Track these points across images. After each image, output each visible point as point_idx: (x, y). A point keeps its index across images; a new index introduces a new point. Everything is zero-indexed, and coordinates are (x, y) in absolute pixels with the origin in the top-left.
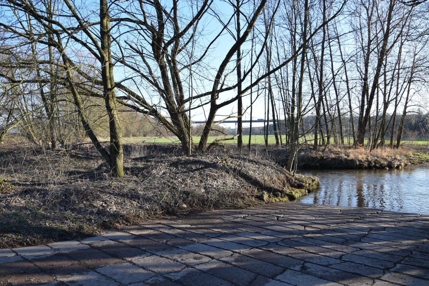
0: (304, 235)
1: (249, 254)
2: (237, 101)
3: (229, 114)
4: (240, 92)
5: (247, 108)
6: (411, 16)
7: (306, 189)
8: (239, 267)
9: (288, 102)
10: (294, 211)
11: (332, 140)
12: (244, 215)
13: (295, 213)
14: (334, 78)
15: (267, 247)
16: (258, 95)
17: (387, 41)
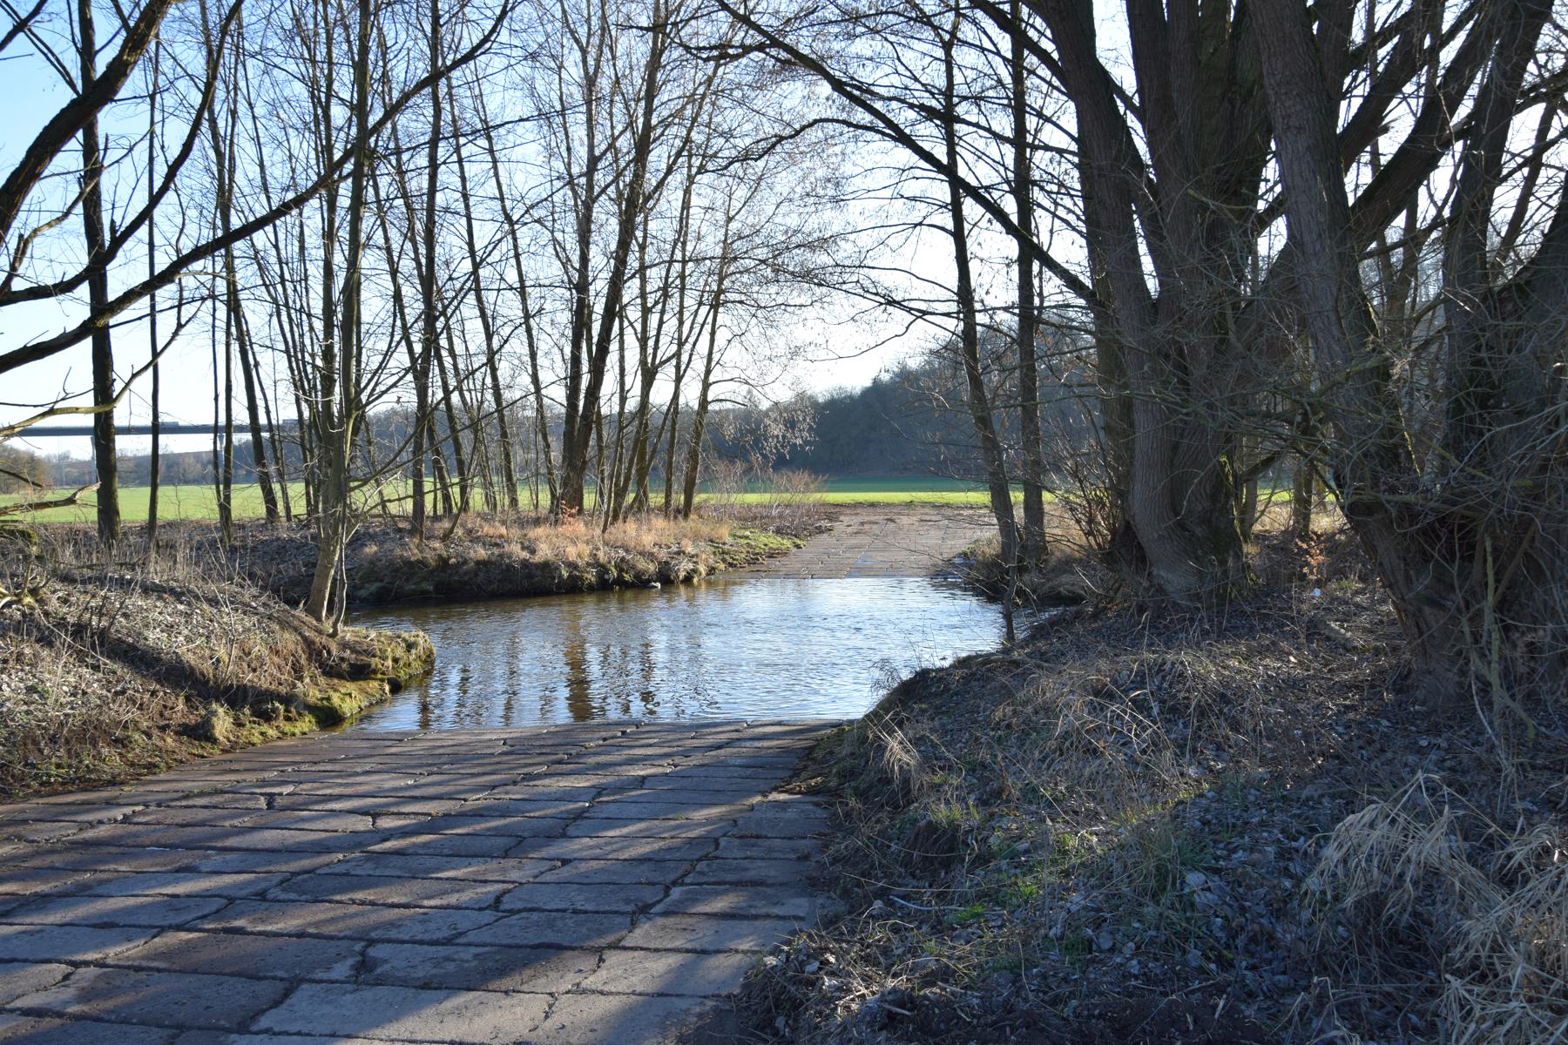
0: (372, 848)
1: (144, 958)
2: (87, 344)
3: (48, 397)
4: (102, 308)
5: (134, 376)
6: (715, 93)
7: (382, 680)
8: (98, 1019)
9: (308, 358)
10: (337, 767)
11: (477, 497)
12: (128, 810)
13: (341, 773)
14: (475, 272)
15: (220, 920)
16: (180, 326)
17: (644, 167)
